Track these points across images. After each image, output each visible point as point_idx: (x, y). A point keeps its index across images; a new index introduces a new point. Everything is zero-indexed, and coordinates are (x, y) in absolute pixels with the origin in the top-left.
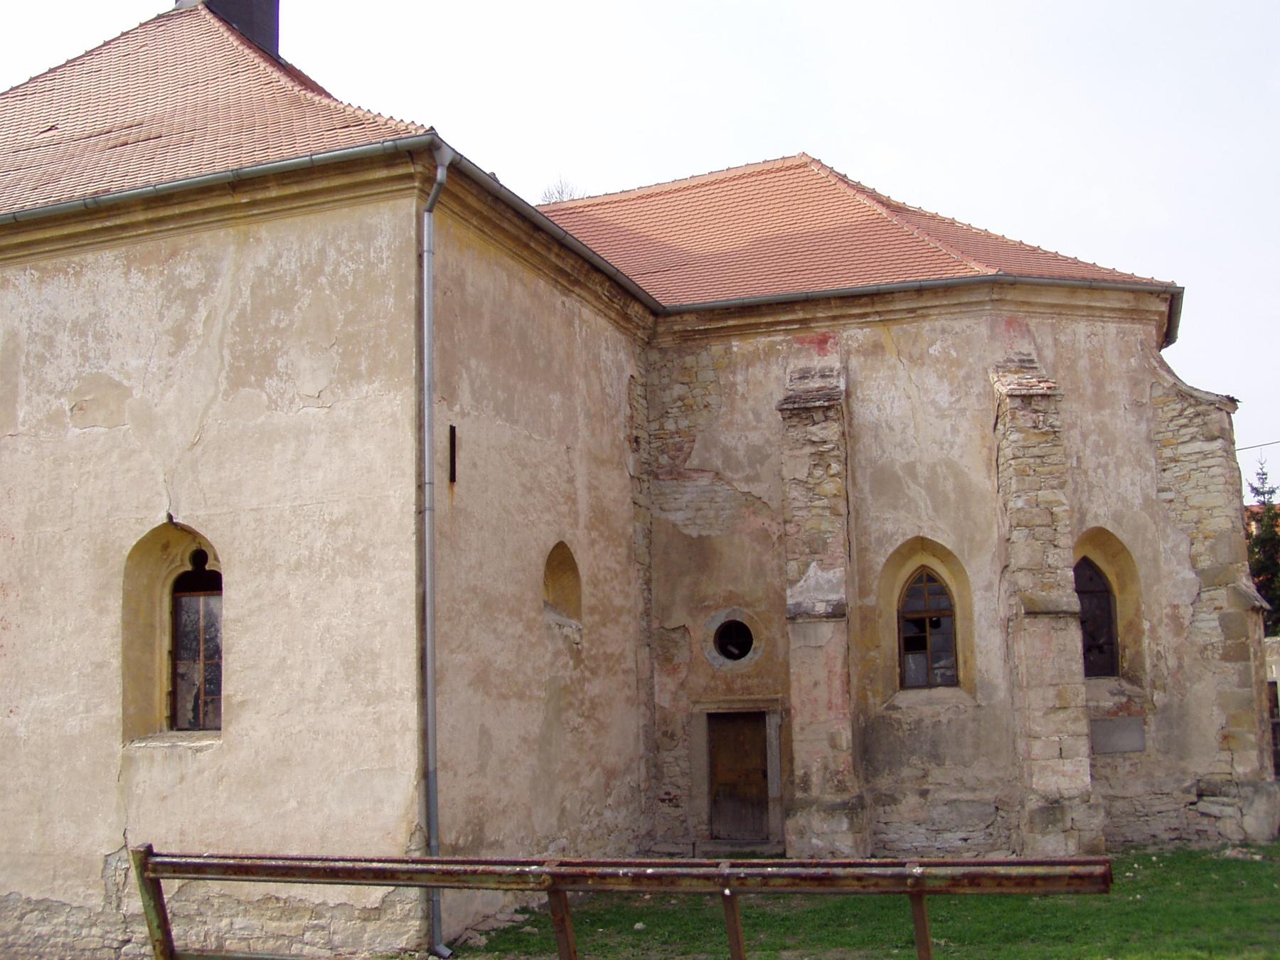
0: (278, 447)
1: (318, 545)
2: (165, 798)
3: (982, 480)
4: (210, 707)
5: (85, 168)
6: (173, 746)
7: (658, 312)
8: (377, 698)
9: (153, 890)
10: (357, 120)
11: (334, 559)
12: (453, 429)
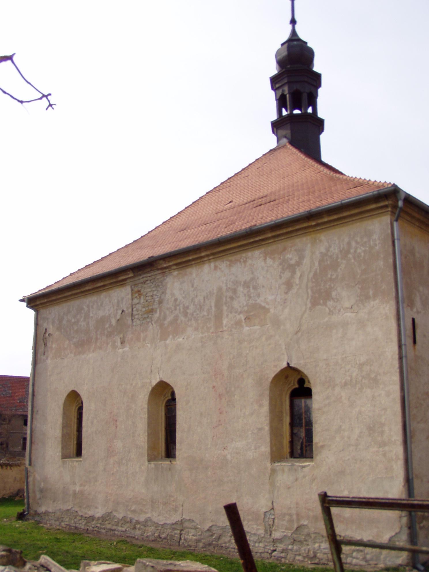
0: (334, 331)
1: (354, 374)
2: (289, 488)
4: (308, 448)
5: (245, 217)
6: (293, 465)
8: (383, 444)
9: (327, 512)
10: (359, 183)
11: (361, 381)
12: (413, 320)
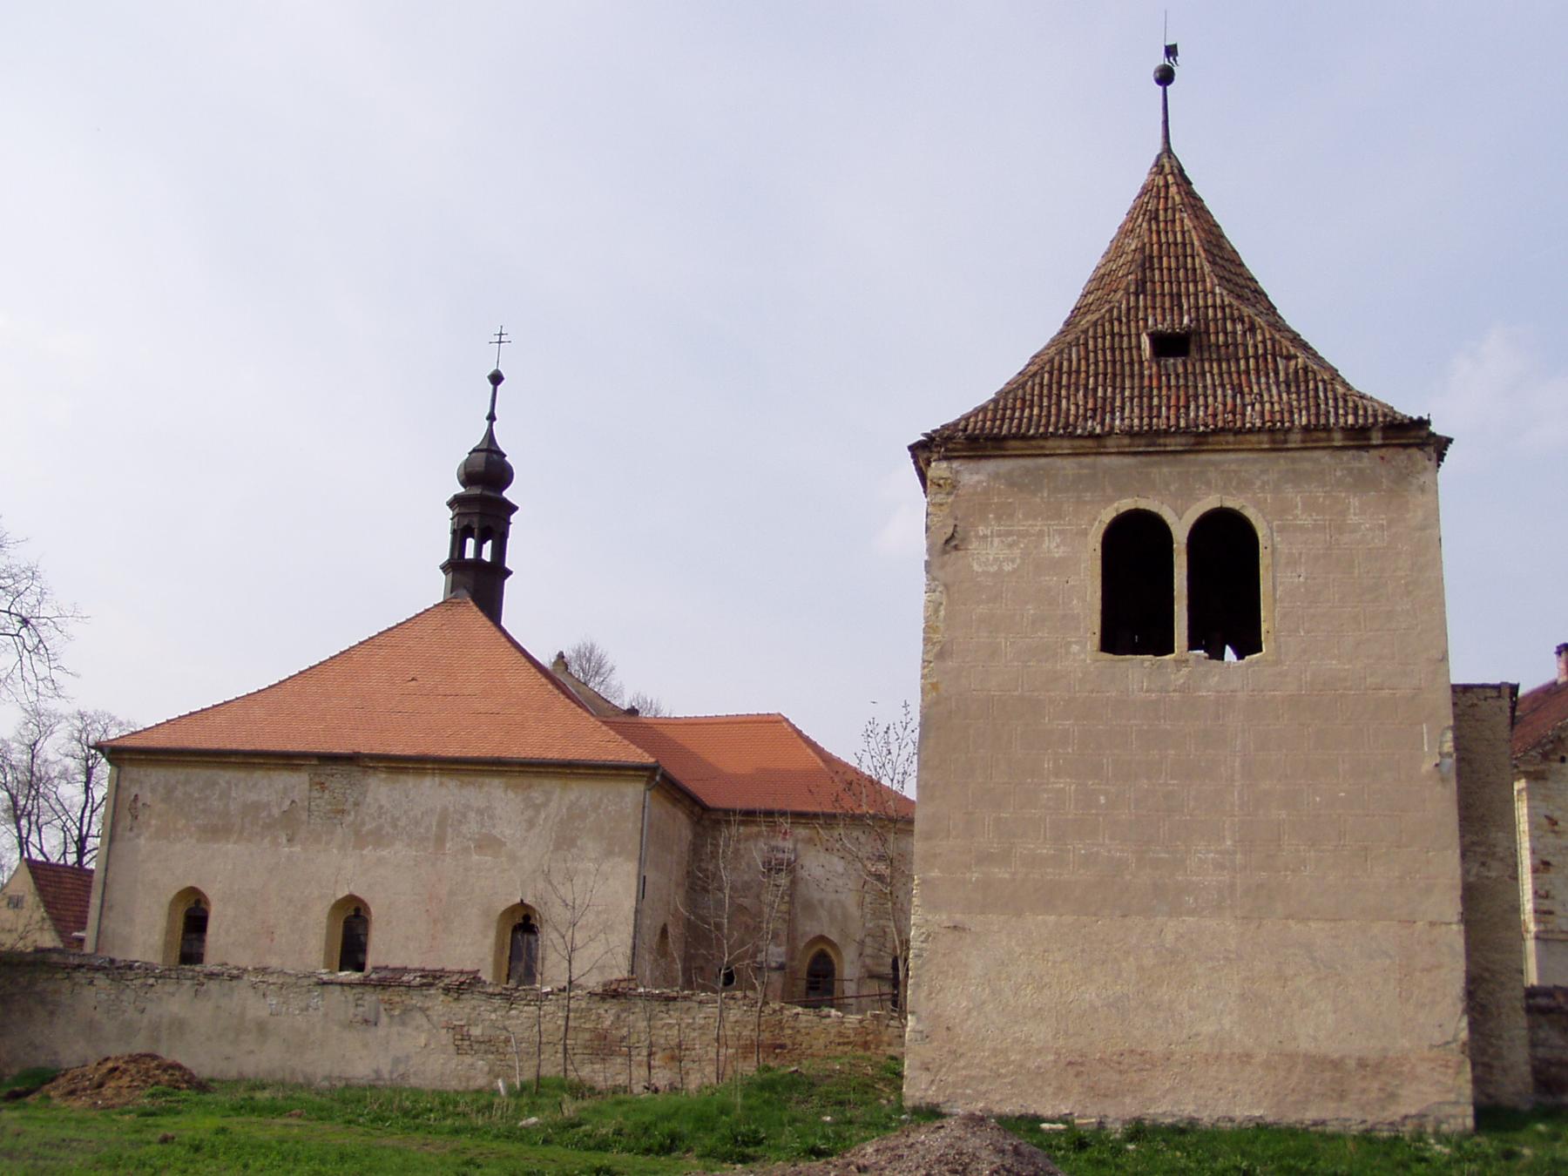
3: (854, 911)
7: (705, 809)
